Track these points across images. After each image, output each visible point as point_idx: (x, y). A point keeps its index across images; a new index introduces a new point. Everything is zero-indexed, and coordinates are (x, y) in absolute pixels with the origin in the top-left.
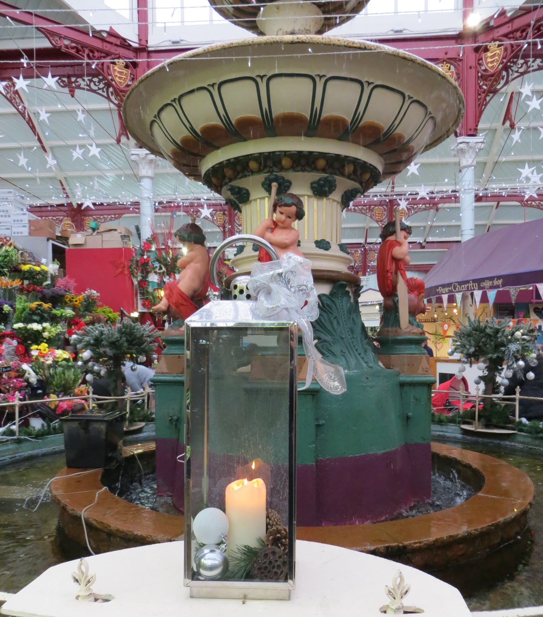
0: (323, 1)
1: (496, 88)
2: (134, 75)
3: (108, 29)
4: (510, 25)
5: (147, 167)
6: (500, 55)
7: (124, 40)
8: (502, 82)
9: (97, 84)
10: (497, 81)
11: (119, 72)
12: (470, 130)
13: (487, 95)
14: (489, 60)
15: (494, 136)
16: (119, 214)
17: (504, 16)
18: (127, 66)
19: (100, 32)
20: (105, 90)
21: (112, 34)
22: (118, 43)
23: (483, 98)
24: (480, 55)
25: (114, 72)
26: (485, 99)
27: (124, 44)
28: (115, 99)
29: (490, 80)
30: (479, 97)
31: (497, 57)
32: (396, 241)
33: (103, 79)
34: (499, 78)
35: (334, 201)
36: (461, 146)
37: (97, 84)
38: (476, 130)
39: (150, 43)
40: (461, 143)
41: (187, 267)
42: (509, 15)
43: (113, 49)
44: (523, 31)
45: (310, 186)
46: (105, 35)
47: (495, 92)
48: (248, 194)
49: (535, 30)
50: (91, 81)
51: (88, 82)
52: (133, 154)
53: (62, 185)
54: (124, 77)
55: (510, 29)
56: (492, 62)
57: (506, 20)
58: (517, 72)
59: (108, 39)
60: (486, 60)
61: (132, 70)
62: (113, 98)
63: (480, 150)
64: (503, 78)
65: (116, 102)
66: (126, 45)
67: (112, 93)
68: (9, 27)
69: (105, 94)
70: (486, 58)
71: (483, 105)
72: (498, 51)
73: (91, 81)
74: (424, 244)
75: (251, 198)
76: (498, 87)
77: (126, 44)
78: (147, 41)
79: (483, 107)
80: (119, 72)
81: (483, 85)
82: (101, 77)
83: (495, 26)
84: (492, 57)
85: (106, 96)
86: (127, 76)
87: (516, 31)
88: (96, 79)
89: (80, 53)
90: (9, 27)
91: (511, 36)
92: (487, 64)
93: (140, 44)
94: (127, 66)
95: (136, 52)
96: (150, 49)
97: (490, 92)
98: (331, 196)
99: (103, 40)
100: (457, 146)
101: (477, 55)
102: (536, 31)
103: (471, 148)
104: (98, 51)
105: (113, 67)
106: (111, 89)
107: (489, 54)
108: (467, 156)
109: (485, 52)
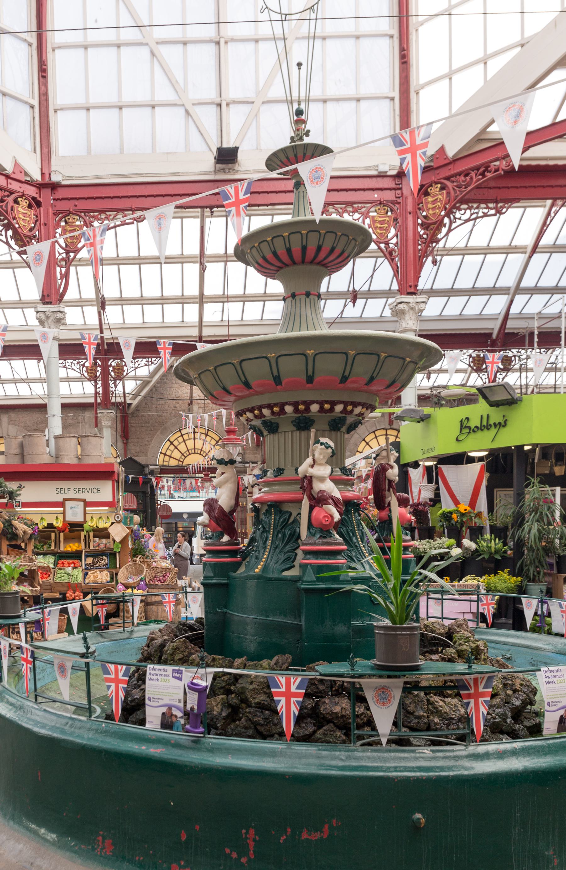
0: (564, 594)
6: (442, 201)
8: (444, 230)
10: (439, 230)
18: (30, 206)
28: (16, 244)
29: (432, 229)
31: (439, 204)
32: (388, 464)
36: (401, 306)
40: (401, 303)
44: (467, 175)
48: (277, 426)
49: (480, 175)
50: (72, 363)
56: (433, 209)
58: (460, 219)
61: (36, 211)
62: (12, 242)
64: (445, 225)
67: (12, 238)
68: (208, 690)
70: (427, 203)
72: (440, 197)
73: (72, 363)
75: (280, 430)
79: (425, 259)
81: (424, 234)
83: (434, 167)
84: (434, 202)
85: (5, 241)
87: (459, 174)
90: (208, 690)
92: (428, 210)
94: (30, 206)
102: (480, 177)
103: (412, 308)
105: (17, 208)
107: (430, 199)
108: (407, 317)
109: (425, 196)
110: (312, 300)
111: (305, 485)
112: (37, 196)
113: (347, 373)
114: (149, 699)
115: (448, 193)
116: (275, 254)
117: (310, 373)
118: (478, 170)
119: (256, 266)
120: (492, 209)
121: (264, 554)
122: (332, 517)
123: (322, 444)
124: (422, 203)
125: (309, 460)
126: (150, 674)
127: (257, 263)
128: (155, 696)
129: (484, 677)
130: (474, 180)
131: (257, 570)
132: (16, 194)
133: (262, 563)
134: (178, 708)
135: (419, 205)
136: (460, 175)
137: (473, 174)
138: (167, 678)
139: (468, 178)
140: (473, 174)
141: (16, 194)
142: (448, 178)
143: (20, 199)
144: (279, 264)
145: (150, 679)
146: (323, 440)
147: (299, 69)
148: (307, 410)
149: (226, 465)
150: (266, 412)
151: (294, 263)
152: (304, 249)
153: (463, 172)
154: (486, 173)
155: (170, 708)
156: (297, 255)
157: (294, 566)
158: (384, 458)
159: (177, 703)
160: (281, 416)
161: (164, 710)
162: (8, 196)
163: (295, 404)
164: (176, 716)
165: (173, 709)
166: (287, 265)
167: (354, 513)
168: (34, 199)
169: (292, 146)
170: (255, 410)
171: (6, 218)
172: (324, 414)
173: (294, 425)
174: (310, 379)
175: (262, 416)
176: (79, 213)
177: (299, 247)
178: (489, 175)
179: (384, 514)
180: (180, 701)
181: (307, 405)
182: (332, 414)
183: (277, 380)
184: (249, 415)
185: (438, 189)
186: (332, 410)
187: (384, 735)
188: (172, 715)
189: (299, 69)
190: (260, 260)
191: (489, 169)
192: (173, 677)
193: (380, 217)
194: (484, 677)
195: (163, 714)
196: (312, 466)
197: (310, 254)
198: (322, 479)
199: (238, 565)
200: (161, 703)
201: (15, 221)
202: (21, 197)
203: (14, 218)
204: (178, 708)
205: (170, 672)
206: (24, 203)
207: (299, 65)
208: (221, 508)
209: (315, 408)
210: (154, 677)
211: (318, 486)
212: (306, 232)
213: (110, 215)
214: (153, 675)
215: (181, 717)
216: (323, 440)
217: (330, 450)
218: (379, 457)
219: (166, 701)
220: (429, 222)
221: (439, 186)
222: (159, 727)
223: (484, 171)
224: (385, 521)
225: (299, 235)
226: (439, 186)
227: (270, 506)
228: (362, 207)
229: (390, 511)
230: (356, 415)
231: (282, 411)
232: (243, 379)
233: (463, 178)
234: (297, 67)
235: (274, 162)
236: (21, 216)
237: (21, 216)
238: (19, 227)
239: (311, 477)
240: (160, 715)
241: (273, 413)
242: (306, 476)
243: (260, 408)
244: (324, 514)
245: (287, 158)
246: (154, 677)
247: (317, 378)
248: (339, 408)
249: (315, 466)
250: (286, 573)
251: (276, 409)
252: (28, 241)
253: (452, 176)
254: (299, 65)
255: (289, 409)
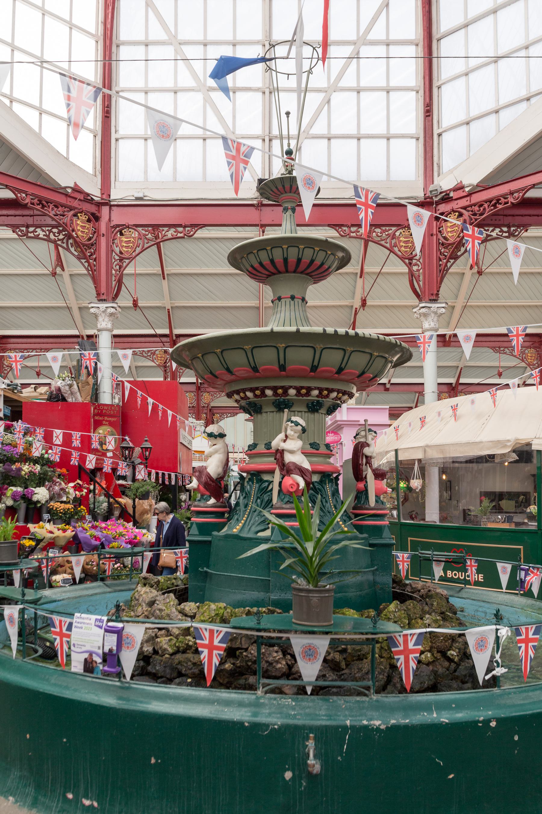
1: (457, 255)
2: (95, 229)
3: (72, 185)
4: (468, 198)
5: (107, 319)
7: (88, 195)
9: (57, 235)
11: (405, 242)
12: (432, 295)
13: (448, 261)
14: (449, 230)
15: (452, 313)
16: (46, 349)
17: (462, 190)
18: (89, 221)
19: (66, 188)
20: (65, 241)
21: (77, 189)
22: (82, 198)
23: (444, 265)
24: (440, 223)
25: (77, 226)
26: (446, 265)
27: (87, 198)
28: (75, 250)
30: (440, 263)
32: (366, 442)
33: (63, 231)
34: (460, 246)
35: (322, 413)
37: (57, 235)
38: (437, 295)
39: (112, 197)
40: (423, 307)
41: (213, 456)
42: (467, 189)
43: (75, 204)
44: (481, 206)
45: (306, 405)
46: (69, 190)
47: (456, 258)
48: (261, 408)
51: (47, 233)
52: (93, 307)
53: (473, 600)
54: (87, 231)
55: (468, 203)
57: (465, 194)
59: (72, 195)
60: (446, 230)
61: (94, 224)
62: (72, 250)
63: (442, 314)
65: (76, 254)
66: (89, 200)
69: (151, 359)
71: (444, 271)
73: (50, 231)
74: (388, 386)
75: (263, 410)
76: (459, 254)
77: (89, 198)
78: (110, 195)
80: (405, 242)
82: (61, 229)
83: (454, 198)
86: (90, 230)
87: (475, 205)
88: (55, 230)
89: (45, 208)
91: (469, 209)
93: (102, 199)
94: (89, 221)
95: (99, 206)
96: (112, 203)
97: (452, 259)
98: (320, 411)
99: (67, 195)
100: (420, 309)
101: (438, 223)
102: (492, 208)
104: (62, 207)
105: (76, 221)
106: (71, 241)
107: (449, 224)
108: (430, 319)
110: (296, 303)
111: (277, 457)
112: (96, 212)
113: (316, 363)
114: (74, 645)
115: (465, 221)
116: (261, 264)
117: (282, 362)
118: (490, 202)
119: (247, 273)
120: (506, 232)
121: (243, 517)
122: (298, 485)
123: (292, 422)
124: (442, 227)
125: (282, 436)
126: (76, 622)
127: (247, 270)
128: (79, 643)
129: (221, 631)
130: (487, 210)
131: (235, 530)
132: (76, 210)
133: (240, 524)
134: (97, 655)
135: (439, 228)
136: (475, 206)
137: (486, 205)
138: (90, 626)
139: (482, 209)
140: (486, 205)
141: (76, 210)
142: (465, 208)
143: (79, 215)
144: (267, 273)
145: (76, 627)
146: (294, 419)
147: (288, 117)
148: (285, 392)
149: (216, 438)
150: (249, 394)
151: (279, 272)
152: (286, 260)
153: (478, 203)
154: (497, 205)
155: (91, 654)
156: (292, 266)
157: (268, 528)
158: (363, 437)
159: (96, 650)
160: (263, 399)
161: (86, 655)
162: (68, 211)
163: (274, 389)
164: (96, 662)
165: (94, 655)
166: (274, 274)
167: (328, 483)
168: (93, 214)
169: (282, 178)
170: (240, 392)
171: (66, 230)
172: (301, 398)
173: (275, 406)
174: (282, 368)
175: (246, 398)
176: (134, 227)
177: (295, 259)
178: (500, 207)
179: (361, 485)
180: (99, 648)
181: (285, 390)
182: (309, 398)
183: (282, 368)
184: (236, 397)
185: (456, 217)
186: (308, 394)
187: (309, 683)
188: (93, 661)
189: (288, 117)
190: (250, 269)
191: (500, 201)
192: (95, 625)
193: (405, 238)
194: (221, 631)
195: (86, 659)
196: (285, 441)
197: (291, 267)
198: (292, 452)
199: (223, 525)
200: (84, 649)
201: (74, 233)
202: (81, 212)
203: (73, 230)
204: (97, 655)
205: (93, 622)
206: (84, 218)
207: (288, 114)
208: (209, 476)
209: (292, 392)
210: (79, 625)
211: (288, 458)
212: (303, 247)
213: (163, 230)
214: (78, 623)
215: (100, 663)
216: (294, 419)
217: (299, 428)
218: (358, 437)
219: (88, 648)
220: (448, 242)
221: (457, 214)
222: (82, 671)
223: (496, 204)
224: (362, 492)
225: (312, 250)
226: (457, 214)
227: (253, 475)
228: (389, 230)
229: (366, 482)
230: (333, 399)
231: (263, 394)
232: (226, 366)
233: (478, 208)
234: (286, 116)
235: (267, 191)
236: (79, 228)
237: (79, 228)
238: (78, 237)
239: (283, 450)
240: (83, 660)
241: (256, 396)
242: (278, 450)
243: (244, 391)
244: (291, 482)
245: (283, 186)
246: (79, 625)
247: (289, 367)
248: (316, 392)
249: (288, 441)
250: (261, 534)
251: (280, 391)
252: (85, 249)
253: (468, 206)
254: (288, 114)
255: (269, 392)
